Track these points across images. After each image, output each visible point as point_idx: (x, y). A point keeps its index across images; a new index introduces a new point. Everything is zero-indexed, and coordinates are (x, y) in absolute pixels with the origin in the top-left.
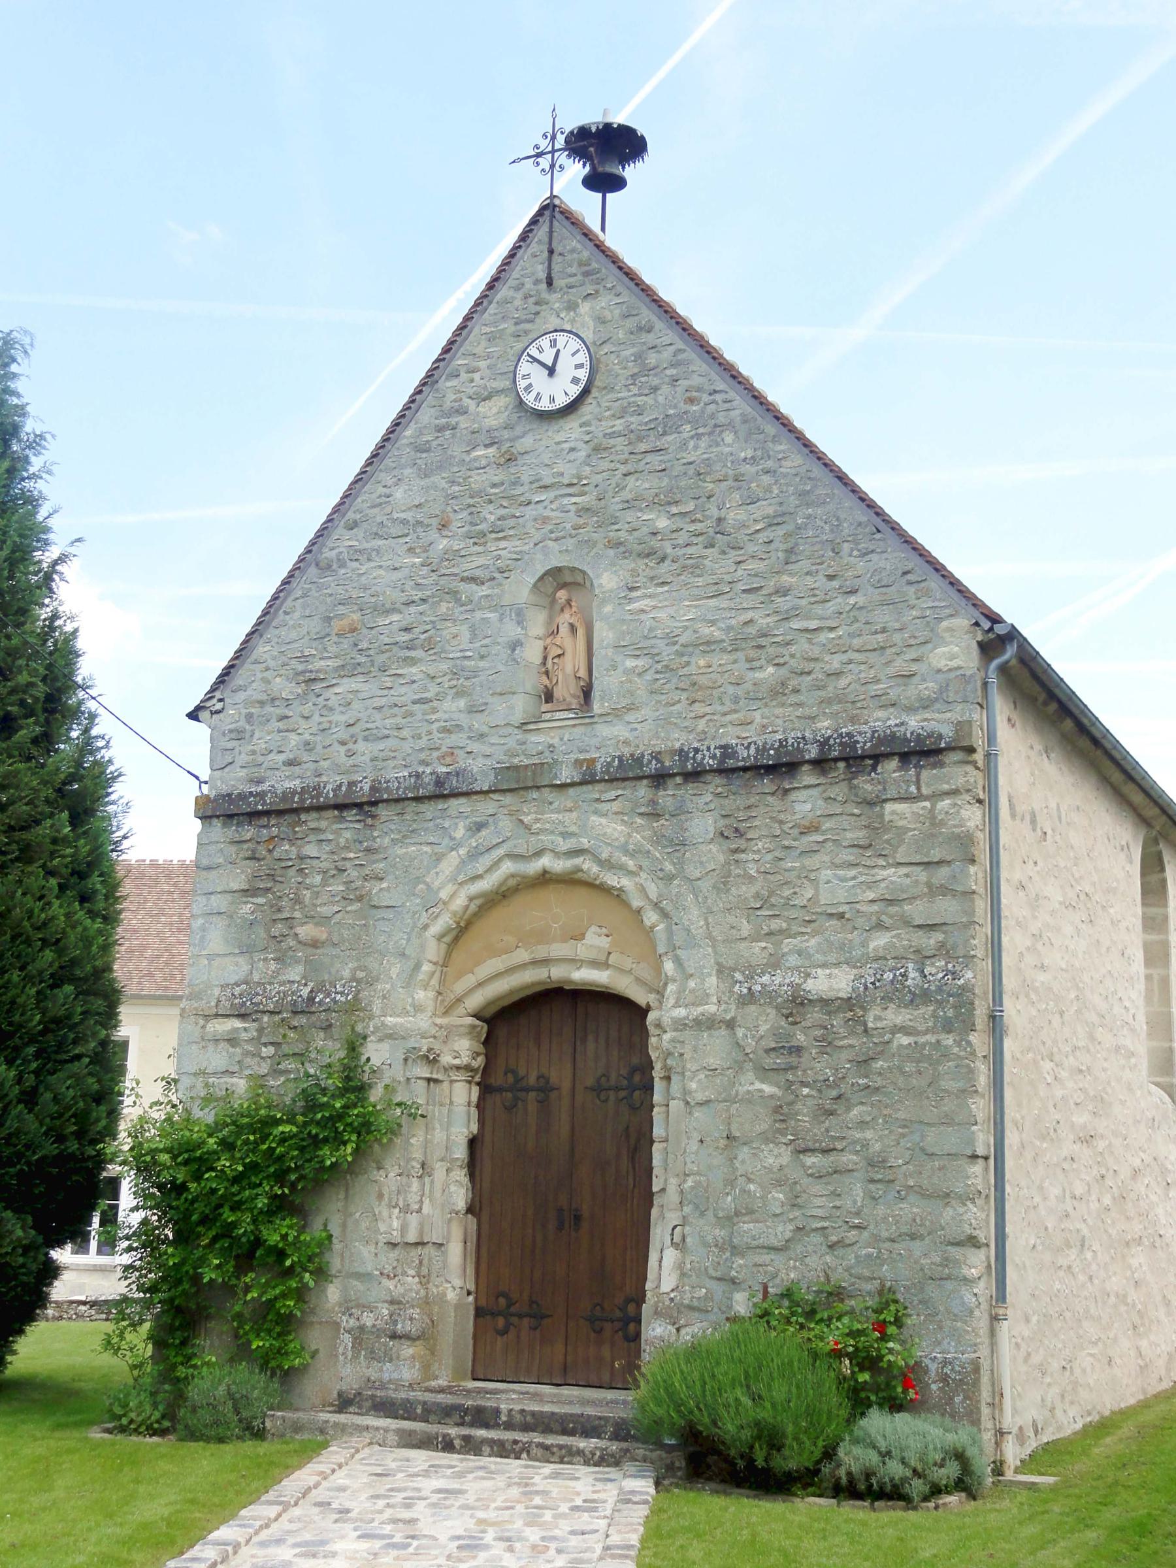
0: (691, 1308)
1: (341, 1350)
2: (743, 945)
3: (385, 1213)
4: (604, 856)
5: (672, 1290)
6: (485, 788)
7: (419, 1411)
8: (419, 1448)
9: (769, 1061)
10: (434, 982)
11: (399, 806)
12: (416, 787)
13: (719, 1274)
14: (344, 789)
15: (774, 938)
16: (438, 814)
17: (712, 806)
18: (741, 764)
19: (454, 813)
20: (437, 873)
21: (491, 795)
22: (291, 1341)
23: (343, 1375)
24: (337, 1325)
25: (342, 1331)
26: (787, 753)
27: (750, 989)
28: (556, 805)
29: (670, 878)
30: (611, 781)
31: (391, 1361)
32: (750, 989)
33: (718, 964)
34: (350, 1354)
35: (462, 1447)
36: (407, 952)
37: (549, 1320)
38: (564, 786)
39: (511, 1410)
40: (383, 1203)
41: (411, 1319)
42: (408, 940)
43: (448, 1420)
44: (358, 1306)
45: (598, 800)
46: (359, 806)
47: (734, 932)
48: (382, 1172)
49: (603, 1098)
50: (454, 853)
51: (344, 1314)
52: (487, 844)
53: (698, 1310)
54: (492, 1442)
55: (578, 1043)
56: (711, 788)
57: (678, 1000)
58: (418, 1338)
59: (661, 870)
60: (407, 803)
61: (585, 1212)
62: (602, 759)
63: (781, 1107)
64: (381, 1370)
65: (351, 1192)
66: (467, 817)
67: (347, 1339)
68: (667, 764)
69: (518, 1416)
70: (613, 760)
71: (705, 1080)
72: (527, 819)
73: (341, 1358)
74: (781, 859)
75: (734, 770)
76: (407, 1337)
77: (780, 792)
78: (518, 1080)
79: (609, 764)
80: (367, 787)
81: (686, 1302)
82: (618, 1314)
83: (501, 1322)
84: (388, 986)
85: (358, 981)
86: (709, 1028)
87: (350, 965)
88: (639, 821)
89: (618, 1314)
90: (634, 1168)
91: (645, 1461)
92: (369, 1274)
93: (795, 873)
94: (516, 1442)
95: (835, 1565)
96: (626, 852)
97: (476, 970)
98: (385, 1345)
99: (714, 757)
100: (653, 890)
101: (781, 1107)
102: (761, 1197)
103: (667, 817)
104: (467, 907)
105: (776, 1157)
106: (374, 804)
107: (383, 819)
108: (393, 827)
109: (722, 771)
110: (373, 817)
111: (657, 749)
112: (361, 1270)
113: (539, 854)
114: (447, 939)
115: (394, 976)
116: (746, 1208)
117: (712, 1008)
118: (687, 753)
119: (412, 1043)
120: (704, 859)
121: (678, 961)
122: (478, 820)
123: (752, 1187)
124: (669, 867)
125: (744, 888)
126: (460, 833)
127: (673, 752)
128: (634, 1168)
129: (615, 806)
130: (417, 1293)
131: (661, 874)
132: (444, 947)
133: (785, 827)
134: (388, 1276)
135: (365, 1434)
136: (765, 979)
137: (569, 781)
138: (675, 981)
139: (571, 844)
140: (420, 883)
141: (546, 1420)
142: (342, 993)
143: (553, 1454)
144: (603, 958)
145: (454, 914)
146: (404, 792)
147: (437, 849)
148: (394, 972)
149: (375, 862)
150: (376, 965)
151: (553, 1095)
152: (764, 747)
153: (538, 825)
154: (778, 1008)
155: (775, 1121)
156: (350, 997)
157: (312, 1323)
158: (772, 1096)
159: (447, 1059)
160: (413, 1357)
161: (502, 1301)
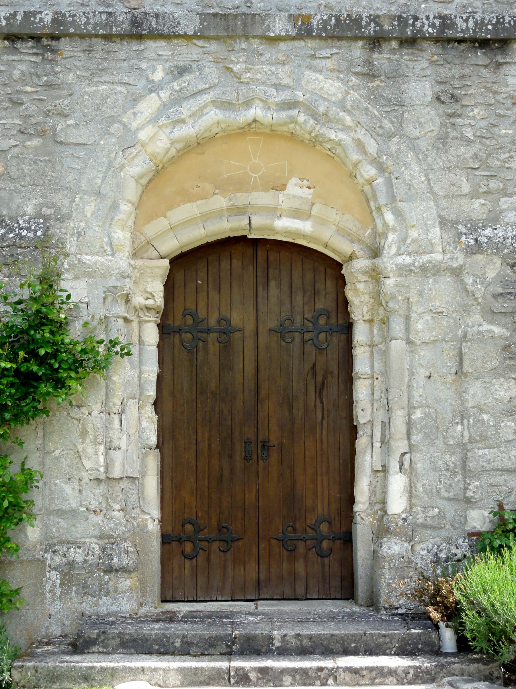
0: (424, 526)
1: (48, 588)
2: (464, 201)
3: (90, 450)
4: (322, 110)
5: (402, 512)
6: (191, 33)
7: (178, 644)
8: (208, 684)
9: (498, 306)
10: (131, 223)
11: (86, 43)
12: (108, 25)
13: (451, 495)
14: (19, 18)
15: (491, 197)
16: (134, 54)
17: (428, 72)
18: (460, 35)
19: (152, 55)
20: (135, 114)
21: (195, 41)
22: (45, 586)
23: (52, 611)
24: (42, 562)
25: (48, 569)
26: (504, 29)
27: (476, 240)
28: (267, 56)
29: (390, 136)
30: (326, 38)
31: (107, 594)
32: (476, 240)
33: (440, 216)
34: (58, 591)
35: (258, 679)
36: (103, 191)
37: (241, 543)
38: (278, 39)
39: (285, 636)
40: (87, 440)
41: (127, 552)
42: (104, 179)
43: (212, 651)
44: (61, 543)
45: (314, 56)
46: (36, 38)
47: (455, 188)
48: (84, 410)
49: (288, 340)
50: (153, 95)
51: (46, 551)
52: (192, 89)
53: (432, 528)
54: (293, 672)
55: (260, 289)
56: (427, 55)
57: (399, 248)
58: (134, 570)
59: (380, 127)
60: (95, 40)
61: (274, 441)
62: (318, 17)
63: (509, 346)
64: (97, 604)
65: (48, 430)
66: (166, 61)
67: (55, 576)
68: (386, 27)
69: (294, 641)
70: (330, 18)
71: (431, 322)
72: (236, 68)
73: (48, 595)
74: (495, 126)
75: (449, 41)
76: (125, 570)
77: (493, 65)
78: (197, 322)
79: (325, 23)
80: (48, 19)
81: (420, 521)
82: (311, 533)
83: (188, 547)
84: (83, 224)
85: (46, 218)
86: (434, 275)
87: (34, 201)
88: (354, 80)
89: (311, 533)
90: (322, 403)
91: (462, 675)
92: (73, 511)
93: (509, 139)
94: (321, 669)
95: (2, 660)
96: (344, 108)
97: (169, 214)
98: (101, 579)
99: (433, 26)
100: (372, 146)
101: (509, 346)
102: (494, 426)
103: (383, 78)
104: (168, 150)
105: (506, 390)
106: (55, 38)
107: (66, 54)
108: (79, 64)
109: (437, 40)
110: (53, 51)
111: (379, 13)
112: (65, 507)
113: (248, 104)
114: (144, 181)
115: (89, 215)
116: (481, 436)
117: (438, 256)
118: (406, 20)
119: (112, 282)
120: (422, 120)
121: (398, 214)
122: (181, 64)
123: (485, 417)
124: (387, 124)
125: (463, 149)
126: (158, 75)
127: (392, 18)
128: (322, 403)
129: (329, 64)
130: (125, 527)
131: (381, 132)
132: (140, 188)
133: (500, 98)
134: (94, 511)
135: (141, 676)
136: (488, 231)
137: (283, 34)
138: (395, 231)
139: (285, 95)
140: (114, 122)
141: (325, 643)
142: (28, 229)
143: (363, 676)
144: (307, 208)
145: (152, 157)
146: (94, 28)
147: (133, 89)
148: (89, 210)
149: (59, 97)
150: (66, 203)
151: (237, 335)
152: (482, 22)
153: (249, 75)
154: (503, 258)
155: (505, 359)
156: (39, 233)
157: (11, 563)
158: (501, 337)
159: (138, 300)
160: (131, 588)
161: (189, 527)
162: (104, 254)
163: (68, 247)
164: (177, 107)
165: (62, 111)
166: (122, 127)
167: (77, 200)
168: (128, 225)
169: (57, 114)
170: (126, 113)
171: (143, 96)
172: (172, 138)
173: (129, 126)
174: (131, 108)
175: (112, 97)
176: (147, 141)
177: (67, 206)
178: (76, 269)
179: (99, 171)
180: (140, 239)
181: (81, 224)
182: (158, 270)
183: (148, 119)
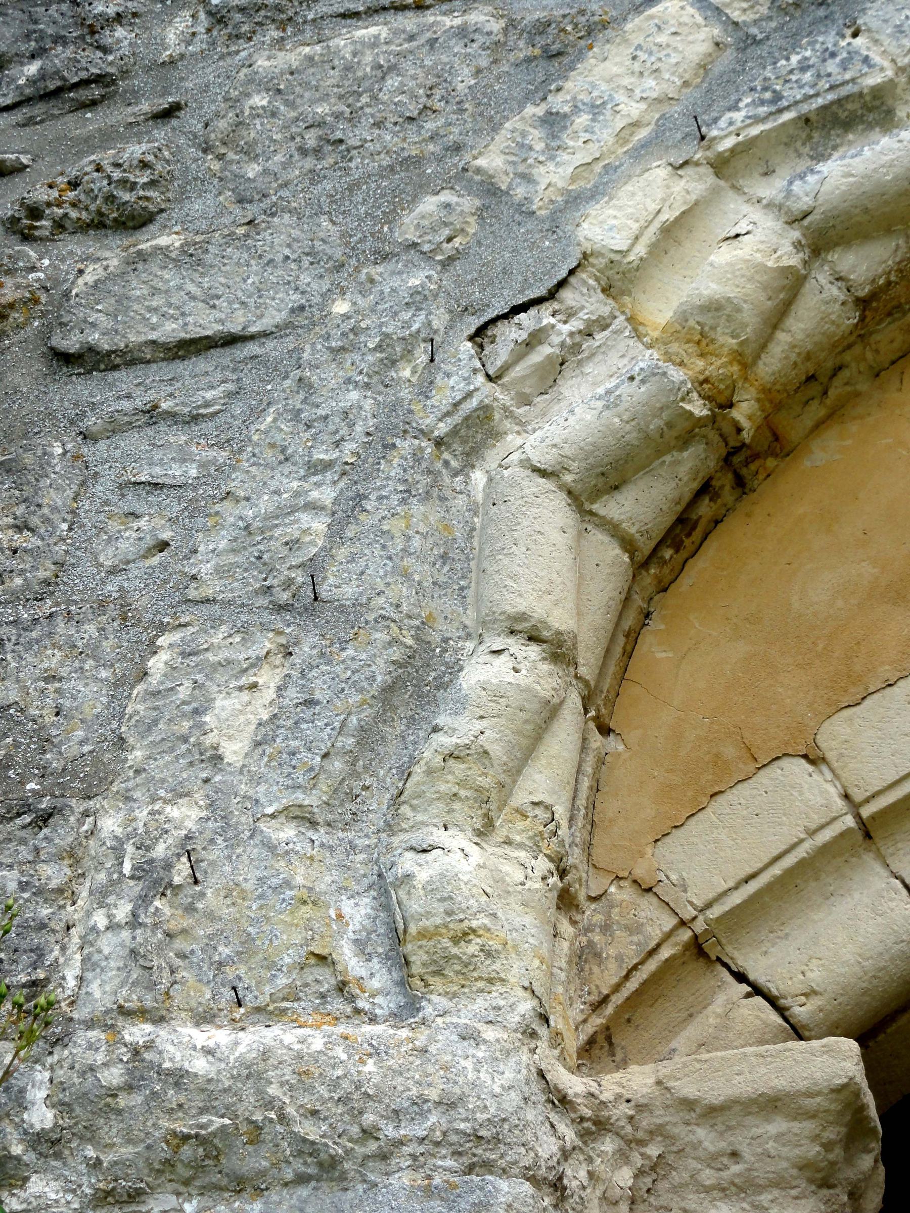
162: (338, 1005)
163: (70, 976)
164: (829, 39)
165: (110, 198)
166: (468, 203)
167: (157, 664)
168: (521, 798)
169: (84, 228)
170: (495, 128)
171: (604, 25)
172: (806, 202)
173: (520, 192)
174: (528, 97)
175: (407, 65)
176: (641, 250)
177: (89, 712)
178: (111, 1131)
179: (317, 468)
180: (634, 929)
181: (173, 812)
182: (778, 1125)
183: (643, 133)
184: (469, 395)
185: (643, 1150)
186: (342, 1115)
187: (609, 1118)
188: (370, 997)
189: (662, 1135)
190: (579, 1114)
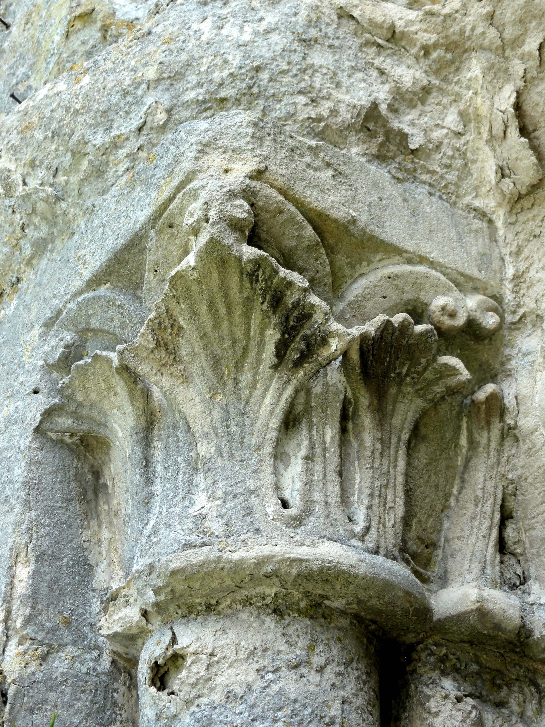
184: (290, 553)
185: (520, 51)
186: (56, 150)
187: (462, 32)
188: (355, 709)
189: (534, 17)
190: (418, 45)
